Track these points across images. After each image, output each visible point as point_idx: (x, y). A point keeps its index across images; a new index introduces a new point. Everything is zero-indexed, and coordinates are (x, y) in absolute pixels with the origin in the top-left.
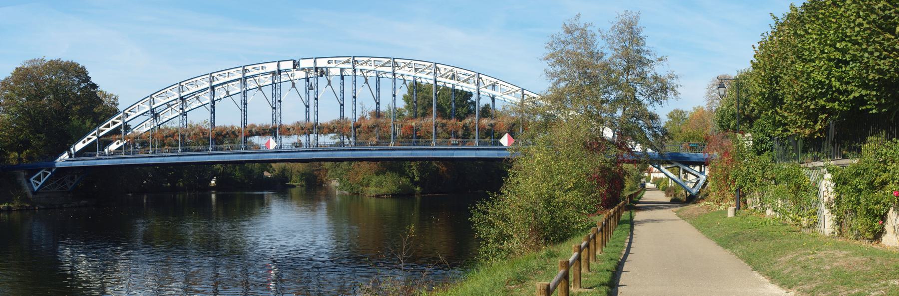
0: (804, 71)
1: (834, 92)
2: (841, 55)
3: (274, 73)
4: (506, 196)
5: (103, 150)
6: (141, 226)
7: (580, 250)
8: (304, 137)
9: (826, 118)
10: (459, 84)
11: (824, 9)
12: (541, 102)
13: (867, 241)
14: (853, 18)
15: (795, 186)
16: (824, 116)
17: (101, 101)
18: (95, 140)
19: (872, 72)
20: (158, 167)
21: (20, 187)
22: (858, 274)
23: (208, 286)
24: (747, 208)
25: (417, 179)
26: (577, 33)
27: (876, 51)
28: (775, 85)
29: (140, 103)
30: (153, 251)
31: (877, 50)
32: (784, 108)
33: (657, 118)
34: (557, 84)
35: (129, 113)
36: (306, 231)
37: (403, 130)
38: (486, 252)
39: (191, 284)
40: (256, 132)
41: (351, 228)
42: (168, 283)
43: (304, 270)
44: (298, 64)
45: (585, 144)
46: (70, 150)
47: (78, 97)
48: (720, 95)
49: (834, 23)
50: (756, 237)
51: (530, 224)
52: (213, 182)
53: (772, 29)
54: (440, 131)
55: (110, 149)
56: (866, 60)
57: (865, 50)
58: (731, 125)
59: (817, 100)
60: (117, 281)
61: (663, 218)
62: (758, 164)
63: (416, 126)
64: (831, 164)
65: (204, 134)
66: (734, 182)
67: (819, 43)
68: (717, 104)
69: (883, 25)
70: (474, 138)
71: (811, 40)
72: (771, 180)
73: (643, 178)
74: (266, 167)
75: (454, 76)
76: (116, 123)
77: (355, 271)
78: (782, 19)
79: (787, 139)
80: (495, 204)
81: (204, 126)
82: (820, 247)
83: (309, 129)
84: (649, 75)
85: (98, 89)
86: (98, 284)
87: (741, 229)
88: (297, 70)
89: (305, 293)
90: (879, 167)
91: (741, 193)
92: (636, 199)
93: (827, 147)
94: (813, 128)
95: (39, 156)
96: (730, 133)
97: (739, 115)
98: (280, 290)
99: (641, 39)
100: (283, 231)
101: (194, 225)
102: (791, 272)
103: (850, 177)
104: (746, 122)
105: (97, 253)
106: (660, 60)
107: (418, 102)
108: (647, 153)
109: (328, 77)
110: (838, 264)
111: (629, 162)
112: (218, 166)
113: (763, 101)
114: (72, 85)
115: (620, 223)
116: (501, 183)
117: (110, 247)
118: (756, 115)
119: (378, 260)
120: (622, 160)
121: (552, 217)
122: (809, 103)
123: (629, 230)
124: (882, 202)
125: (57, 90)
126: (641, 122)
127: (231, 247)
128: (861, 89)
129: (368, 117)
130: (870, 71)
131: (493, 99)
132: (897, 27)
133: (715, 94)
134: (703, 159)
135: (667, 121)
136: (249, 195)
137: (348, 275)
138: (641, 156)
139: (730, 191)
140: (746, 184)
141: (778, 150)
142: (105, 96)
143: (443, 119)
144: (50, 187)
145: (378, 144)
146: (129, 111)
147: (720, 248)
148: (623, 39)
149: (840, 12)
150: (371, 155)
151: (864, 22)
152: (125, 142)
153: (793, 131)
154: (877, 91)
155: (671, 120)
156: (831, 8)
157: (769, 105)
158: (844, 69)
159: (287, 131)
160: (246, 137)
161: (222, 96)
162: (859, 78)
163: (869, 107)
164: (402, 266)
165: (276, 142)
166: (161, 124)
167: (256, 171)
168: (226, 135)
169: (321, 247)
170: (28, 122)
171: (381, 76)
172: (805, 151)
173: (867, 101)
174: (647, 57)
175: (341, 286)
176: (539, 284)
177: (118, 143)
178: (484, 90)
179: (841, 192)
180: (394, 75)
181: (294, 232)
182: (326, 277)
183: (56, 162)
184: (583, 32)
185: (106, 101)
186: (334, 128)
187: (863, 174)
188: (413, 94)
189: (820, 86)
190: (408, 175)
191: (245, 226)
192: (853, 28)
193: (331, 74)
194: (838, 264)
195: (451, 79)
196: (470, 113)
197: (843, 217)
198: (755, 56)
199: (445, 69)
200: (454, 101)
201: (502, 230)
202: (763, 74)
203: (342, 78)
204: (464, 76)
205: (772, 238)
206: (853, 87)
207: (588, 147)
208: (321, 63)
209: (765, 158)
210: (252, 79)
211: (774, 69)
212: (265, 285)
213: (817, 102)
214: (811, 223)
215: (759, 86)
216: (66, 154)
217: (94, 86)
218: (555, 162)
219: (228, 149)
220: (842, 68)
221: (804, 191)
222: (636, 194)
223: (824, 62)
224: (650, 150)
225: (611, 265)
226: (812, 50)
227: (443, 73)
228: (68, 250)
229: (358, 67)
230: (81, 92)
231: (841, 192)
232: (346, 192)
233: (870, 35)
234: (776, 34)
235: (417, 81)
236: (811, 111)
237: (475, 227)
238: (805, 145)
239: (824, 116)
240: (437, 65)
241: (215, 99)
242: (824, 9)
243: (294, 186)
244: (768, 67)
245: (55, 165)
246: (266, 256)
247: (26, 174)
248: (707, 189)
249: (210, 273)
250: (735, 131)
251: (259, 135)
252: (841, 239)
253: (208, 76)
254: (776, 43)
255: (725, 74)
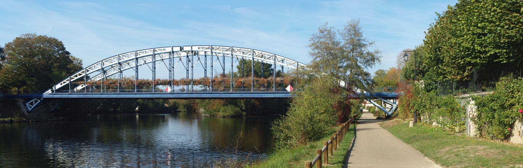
0: (457, 43)
1: (476, 53)
2: (481, 31)
3: (170, 53)
4: (289, 117)
5: (73, 89)
6: (96, 132)
7: (327, 144)
8: (186, 86)
9: (471, 69)
10: (265, 60)
11: (470, 5)
12: (307, 68)
13: (499, 140)
14: (489, 7)
15: (451, 108)
16: (469, 68)
17: (72, 62)
18: (68, 84)
19: (503, 38)
20: (106, 100)
21: (19, 108)
22: (493, 160)
23: (134, 164)
24: (421, 121)
25: (244, 108)
26: (326, 33)
27: (505, 25)
28: (438, 52)
29: (95, 65)
30: (103, 145)
31: (506, 24)
32: (444, 65)
33: (369, 75)
34: (315, 59)
35: (89, 70)
36: (187, 134)
37: (237, 83)
38: (279, 146)
39: (124, 163)
40: (161, 83)
41: (210, 133)
42: (112, 163)
43: (186, 155)
44: (183, 49)
45: (330, 90)
46: (52, 88)
47: (58, 59)
48: (405, 60)
49: (476, 12)
50: (426, 138)
51: (301, 131)
52: (137, 108)
53: (436, 21)
54: (255, 84)
55: (77, 89)
56: (499, 31)
57: (498, 26)
58: (412, 76)
59: (465, 59)
60: (81, 162)
61: (372, 128)
62: (428, 97)
63: (243, 81)
64: (474, 95)
65: (132, 83)
66: (413, 108)
67: (466, 26)
68: (403, 66)
69: (511, 8)
70: (273, 87)
71: (461, 24)
72: (436, 106)
73: (361, 107)
74: (166, 101)
75: (262, 56)
76: (81, 74)
77: (212, 155)
78: (442, 14)
79: (445, 82)
80: (284, 121)
81: (132, 79)
82: (467, 144)
83: (188, 82)
84: (365, 52)
85: (70, 55)
86: (70, 164)
87: (417, 133)
88: (182, 52)
89: (186, 167)
90: (508, 95)
91: (417, 114)
92: (358, 118)
93: (472, 85)
94: (463, 75)
95: (32, 91)
96: (411, 81)
97: (416, 71)
98: (173, 165)
99: (360, 34)
100: (175, 135)
101: (127, 131)
102: (448, 158)
103: (488, 102)
104: (420, 74)
105: (69, 147)
106: (371, 44)
107: (244, 69)
108: (364, 93)
109: (198, 56)
110: (479, 153)
111: (354, 98)
112: (140, 100)
113: (431, 62)
114: (54, 51)
115: (349, 130)
116: (287, 110)
117: (77, 143)
118: (426, 70)
119: (224, 149)
120: (350, 98)
121: (313, 127)
122: (460, 61)
123: (354, 134)
124: (510, 116)
125: (44, 53)
126: (360, 77)
127: (147, 143)
128: (495, 49)
129: (219, 76)
130: (502, 38)
131: (283, 68)
132: (521, 8)
133: (402, 60)
134: (395, 96)
135: (375, 76)
136: (157, 116)
137: (209, 157)
138: (360, 95)
139: (411, 113)
140: (420, 108)
141: (440, 89)
142: (74, 59)
143: (257, 78)
144: (39, 109)
145: (224, 90)
146: (89, 68)
147: (405, 144)
148: (350, 34)
149: (481, 6)
150: (220, 96)
151: (497, 9)
152: (87, 85)
153: (449, 77)
154: (507, 49)
155: (377, 75)
156: (474, 4)
157: (435, 64)
158: (483, 39)
159: (177, 83)
160: (155, 85)
161: (142, 64)
162: (494, 43)
163: (501, 59)
164: (236, 152)
165: (171, 88)
166: (108, 76)
167: (161, 103)
168: (144, 84)
169: (195, 143)
170: (24, 70)
171: (225, 56)
172: (457, 88)
173: (500, 56)
174: (364, 43)
175: (205, 163)
176: (306, 162)
177: (82, 86)
178: (278, 63)
179: (481, 111)
180: (232, 55)
181: (181, 135)
182: (197, 158)
183: (43, 95)
184: (329, 32)
185: (75, 62)
186: (201, 82)
187: (497, 100)
188: (242, 65)
189: (467, 50)
190: (239, 106)
191: (154, 132)
192: (490, 13)
193: (200, 54)
194: (479, 153)
195: (261, 57)
196: (271, 75)
197: (482, 126)
198: (426, 37)
199: (258, 52)
200: (263, 69)
201: (287, 134)
202: (431, 47)
203: (206, 56)
204: (267, 56)
205: (436, 138)
206: (490, 49)
207: (332, 91)
208: (195, 49)
209: (432, 94)
210: (158, 55)
211: (438, 43)
212: (165, 163)
213: (465, 59)
214: (461, 130)
215: (428, 54)
216: (50, 90)
217: (68, 53)
218: (314, 99)
219: (146, 92)
220: (482, 38)
221: (457, 111)
222: (357, 115)
223: (470, 36)
224: (365, 92)
225: (344, 152)
226: (462, 30)
227: (257, 54)
228: (51, 145)
229: (214, 51)
230: (59, 56)
231: (481, 111)
232: (207, 115)
233: (501, 16)
234: (439, 24)
235: (244, 58)
236: (461, 65)
237: (273, 132)
238: (457, 85)
239: (469, 68)
240: (254, 51)
241: (138, 65)
242: (470, 5)
243: (181, 112)
244: (434, 42)
245: (42, 96)
246: (166, 148)
247: (23, 101)
248: (397, 112)
249: (135, 157)
250: (414, 79)
251: (162, 84)
252: (481, 139)
253: (134, 52)
254: (439, 28)
255: (408, 49)
